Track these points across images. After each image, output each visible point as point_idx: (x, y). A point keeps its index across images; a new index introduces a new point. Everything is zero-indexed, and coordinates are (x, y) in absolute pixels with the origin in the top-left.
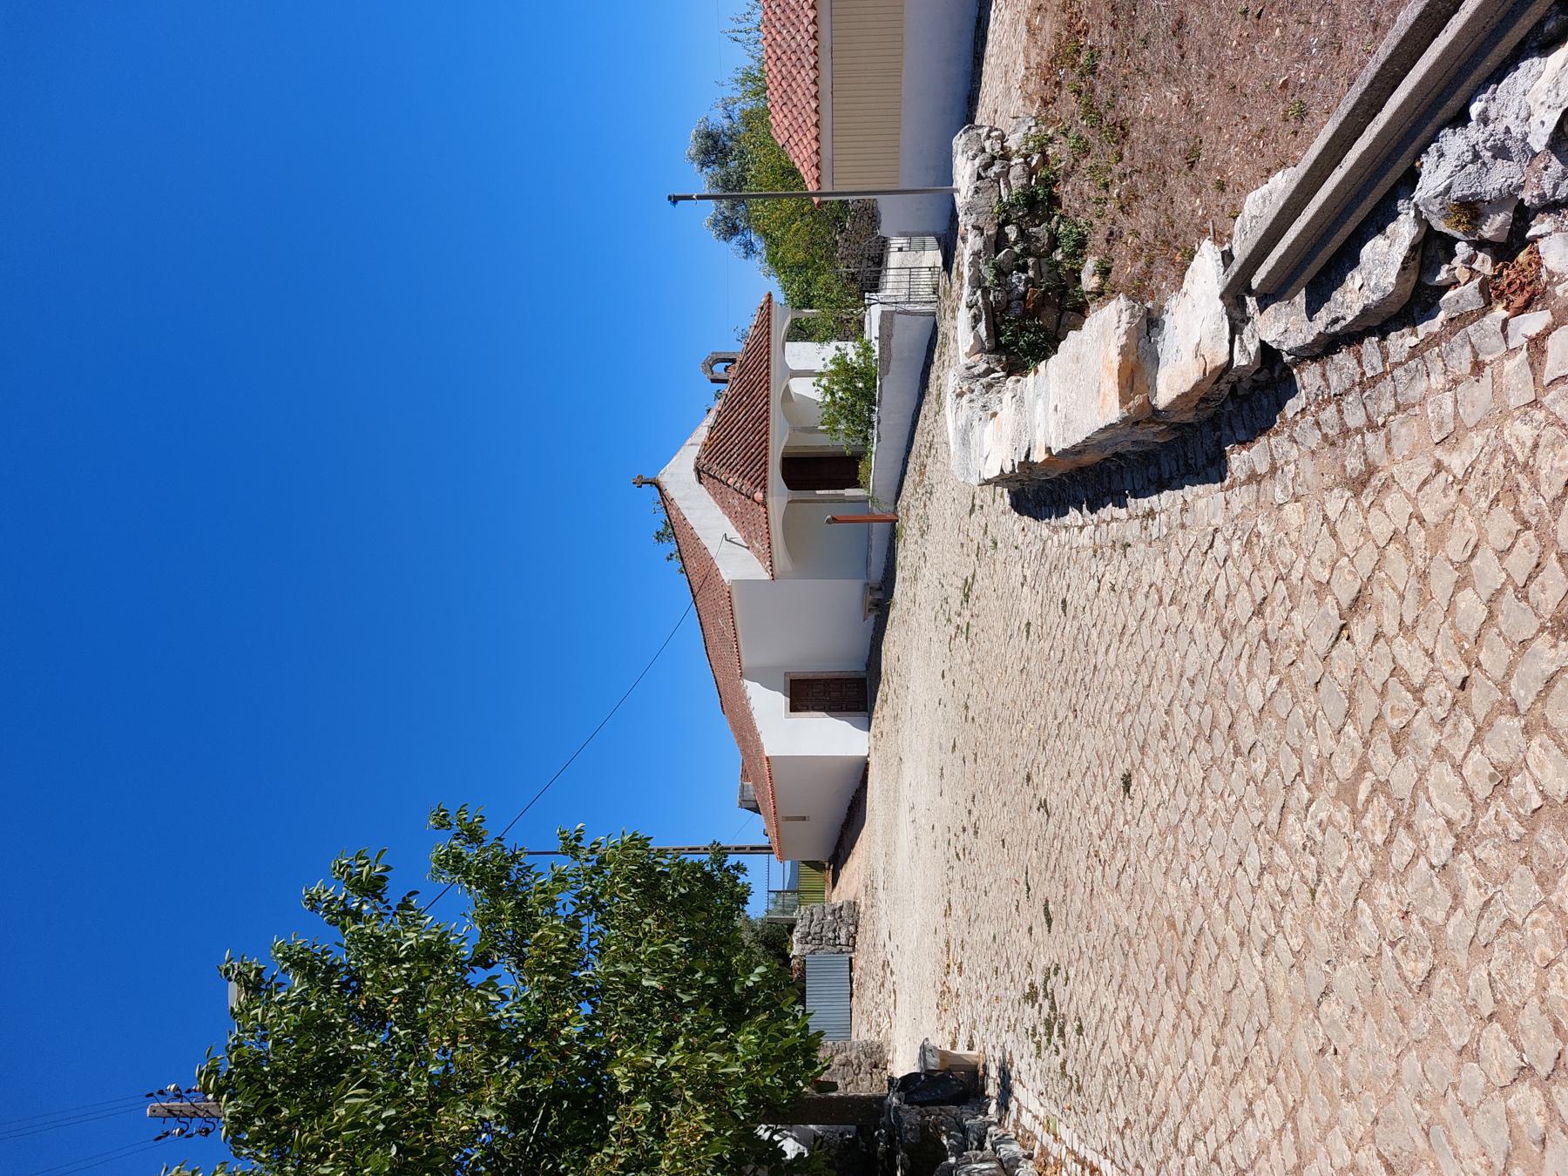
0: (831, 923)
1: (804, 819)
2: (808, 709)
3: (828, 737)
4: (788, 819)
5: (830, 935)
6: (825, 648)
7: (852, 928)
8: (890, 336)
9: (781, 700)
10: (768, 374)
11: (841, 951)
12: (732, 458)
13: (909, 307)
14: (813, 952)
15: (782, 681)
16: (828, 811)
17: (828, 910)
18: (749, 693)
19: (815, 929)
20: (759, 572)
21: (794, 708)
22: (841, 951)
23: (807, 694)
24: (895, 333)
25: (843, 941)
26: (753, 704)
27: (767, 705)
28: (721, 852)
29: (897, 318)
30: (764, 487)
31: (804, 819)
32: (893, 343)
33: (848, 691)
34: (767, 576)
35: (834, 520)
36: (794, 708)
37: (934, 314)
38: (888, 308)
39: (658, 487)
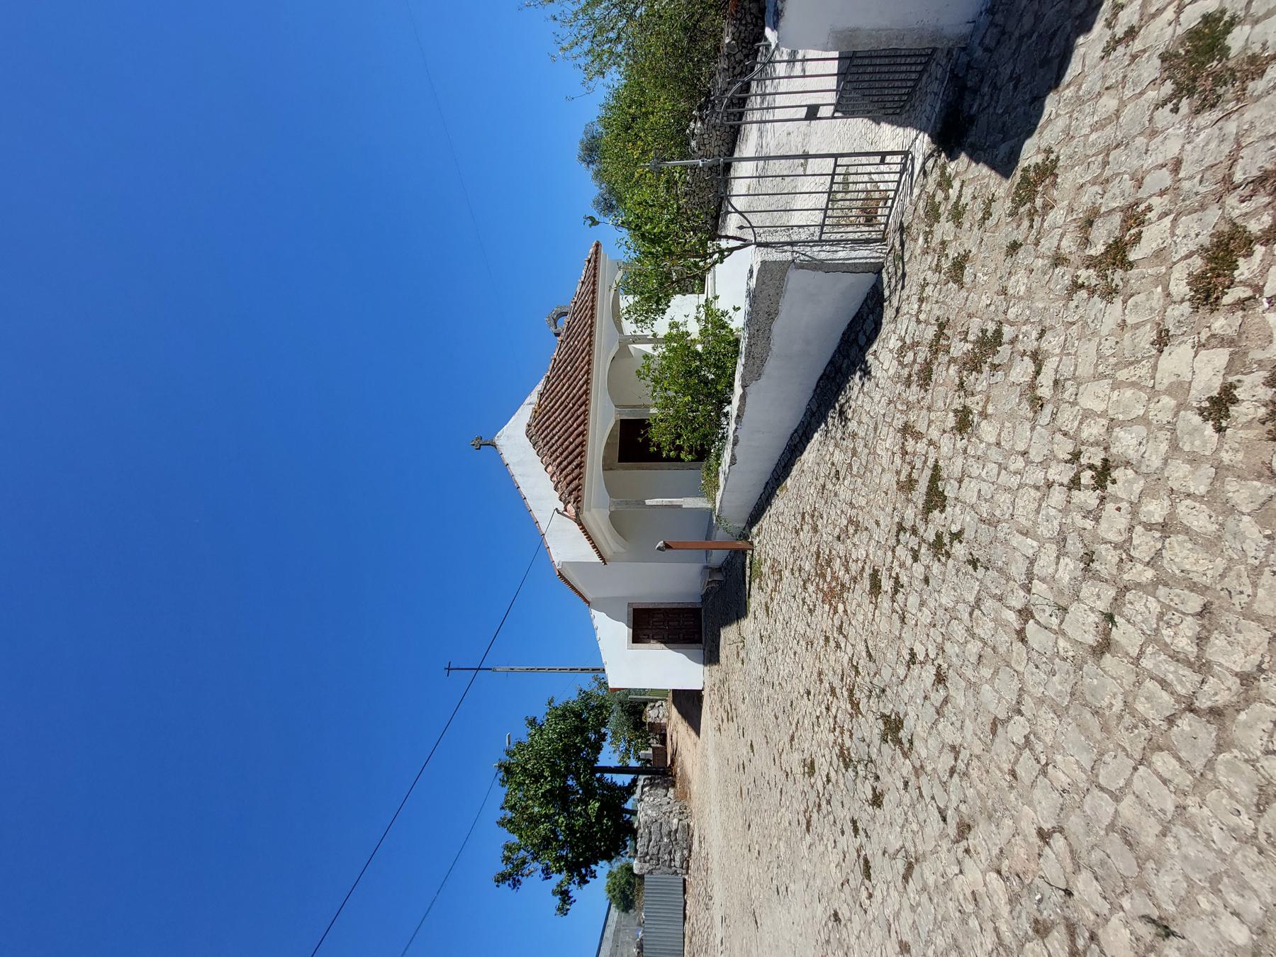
0: (667, 845)
3: (663, 668)
5: (666, 857)
8: (772, 315)
9: (624, 631)
10: (590, 344)
12: (560, 442)
13: (822, 254)
14: (650, 872)
15: (625, 611)
17: (665, 830)
18: (596, 623)
19: (653, 851)
21: (637, 639)
23: (649, 624)
24: (784, 306)
25: (678, 864)
26: (599, 634)
27: (612, 633)
29: (795, 279)
30: (577, 500)
32: (777, 327)
33: (688, 624)
35: (667, 546)
36: (637, 639)
37: (878, 269)
38: (774, 255)
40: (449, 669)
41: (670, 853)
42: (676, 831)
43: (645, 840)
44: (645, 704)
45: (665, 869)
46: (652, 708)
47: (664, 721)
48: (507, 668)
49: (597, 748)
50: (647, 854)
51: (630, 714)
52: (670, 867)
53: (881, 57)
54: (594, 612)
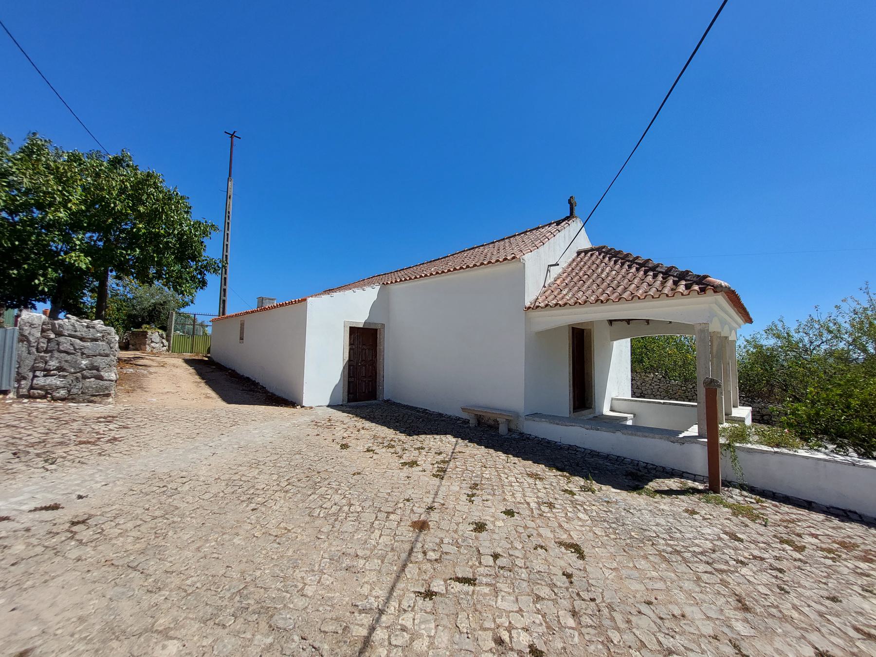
0: (75, 365)
1: (242, 339)
2: (574, 391)
3: (322, 368)
4: (242, 325)
5: (53, 364)
6: (407, 369)
7: (63, 393)
9: (360, 319)
11: (20, 378)
15: (378, 320)
16: (250, 358)
17: (99, 361)
18: (368, 289)
19: (65, 343)
20: (532, 293)
21: (354, 332)
22: (20, 378)
23: (365, 342)
25: (41, 381)
27: (357, 305)
28: (221, 268)
31: (242, 339)
33: (365, 387)
34: (528, 304)
36: (354, 332)
39: (567, 218)
40: (232, 136)
41: (60, 369)
42: (100, 378)
43: (82, 332)
44: (164, 328)
45: (29, 362)
46: (161, 336)
47: (148, 349)
48: (231, 192)
49: (81, 269)
50: (59, 334)
51: (150, 312)
52: (34, 369)
53: (670, 492)
54: (378, 288)
